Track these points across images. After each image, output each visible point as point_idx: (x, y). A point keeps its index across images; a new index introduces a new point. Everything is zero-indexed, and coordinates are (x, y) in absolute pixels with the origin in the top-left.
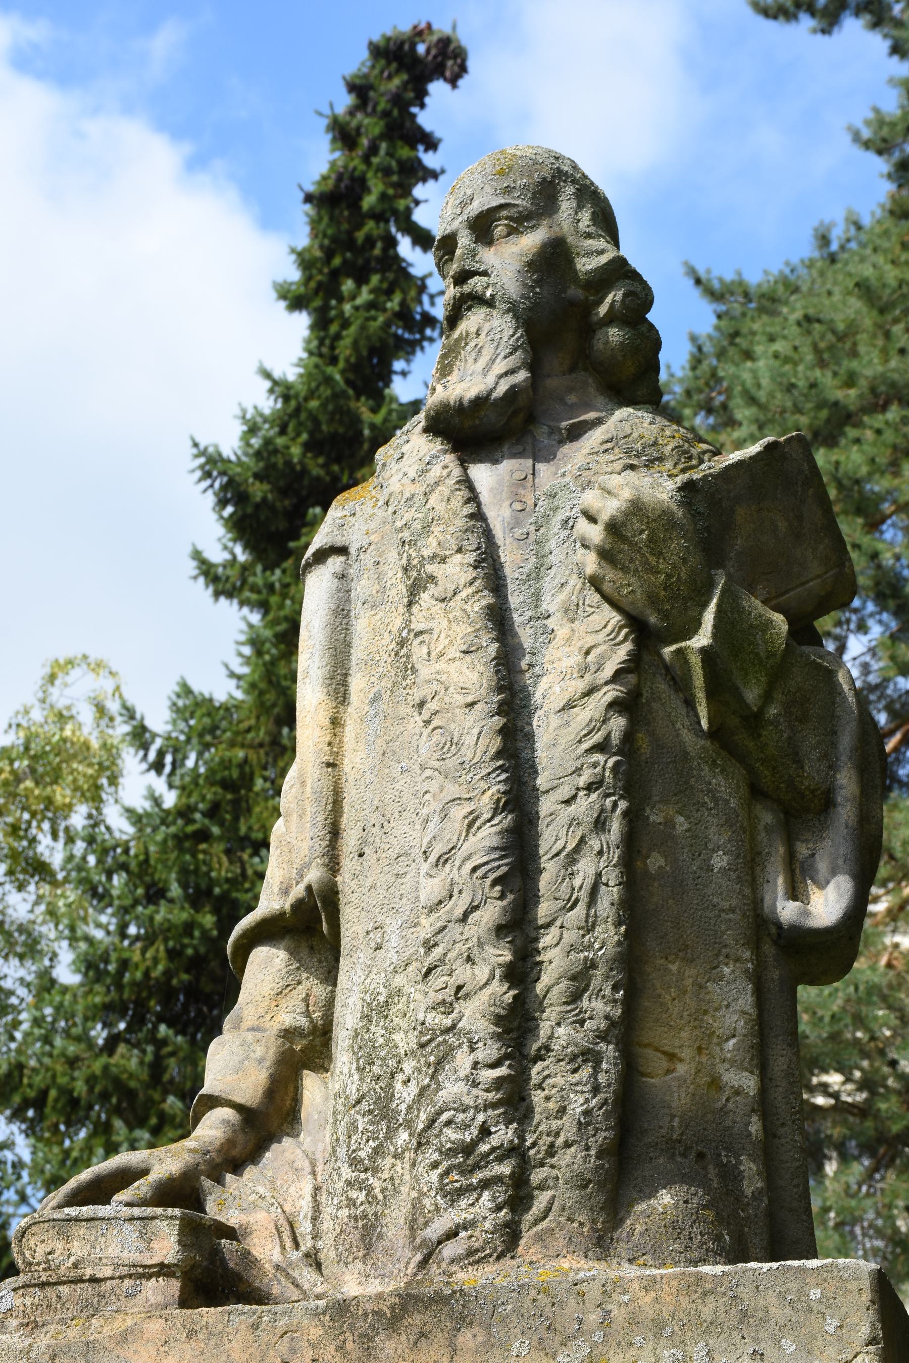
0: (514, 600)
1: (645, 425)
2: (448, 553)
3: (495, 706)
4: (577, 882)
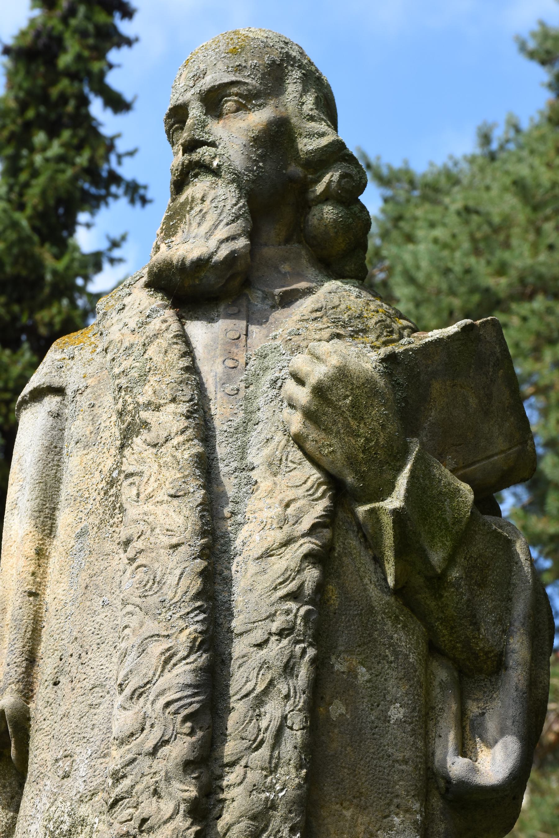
0: (221, 451)
1: (352, 298)
2: (162, 402)
3: (198, 549)
4: (264, 724)
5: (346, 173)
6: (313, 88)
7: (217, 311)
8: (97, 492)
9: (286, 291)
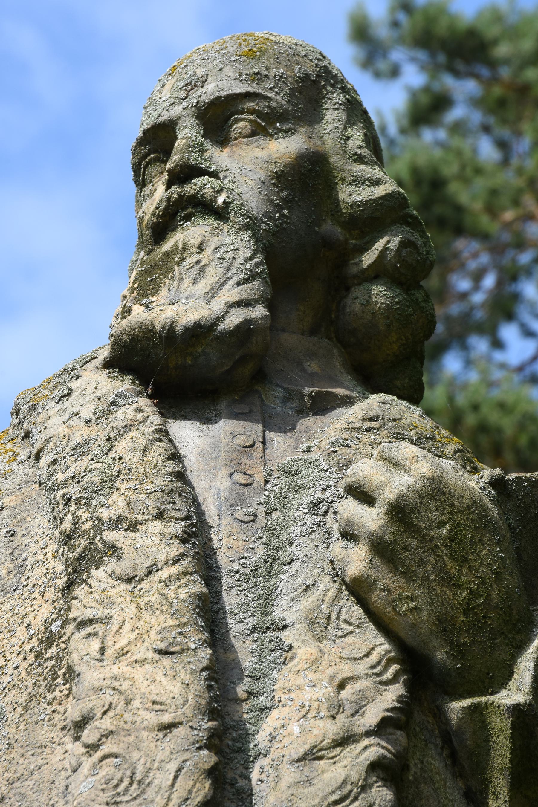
2: (141, 518)
3: (205, 734)
5: (409, 241)
6: (360, 122)
7: (215, 410)
8: (21, 656)
9: (319, 391)
